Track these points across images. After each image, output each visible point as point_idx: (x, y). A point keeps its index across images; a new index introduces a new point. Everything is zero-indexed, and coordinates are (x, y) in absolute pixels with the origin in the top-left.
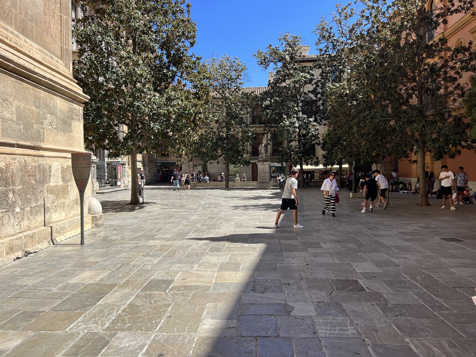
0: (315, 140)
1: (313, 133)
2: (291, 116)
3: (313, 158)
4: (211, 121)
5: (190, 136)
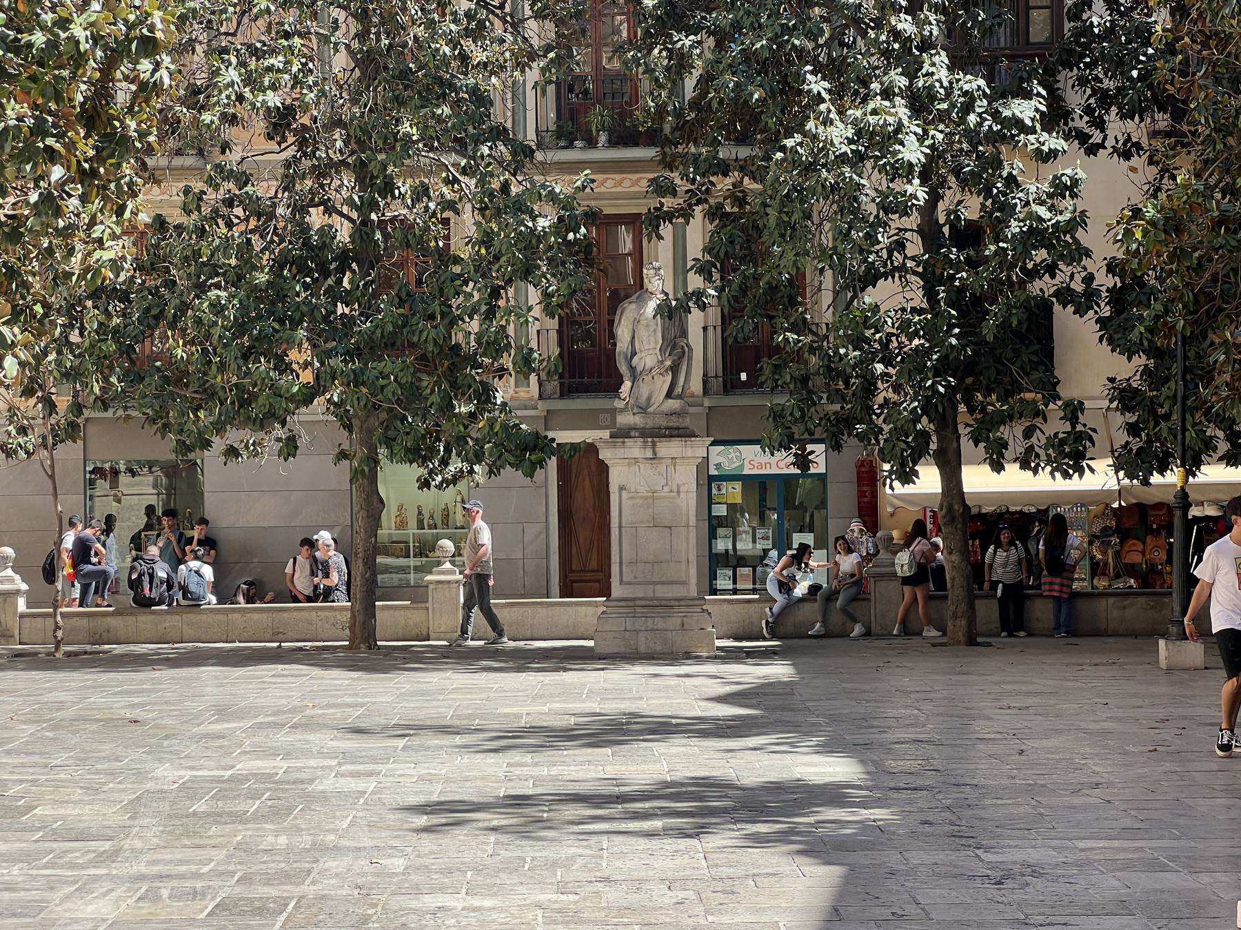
0: (1052, 270)
1: (1042, 212)
2: (865, 83)
3: (1037, 413)
4: (232, 120)
5: (59, 232)
